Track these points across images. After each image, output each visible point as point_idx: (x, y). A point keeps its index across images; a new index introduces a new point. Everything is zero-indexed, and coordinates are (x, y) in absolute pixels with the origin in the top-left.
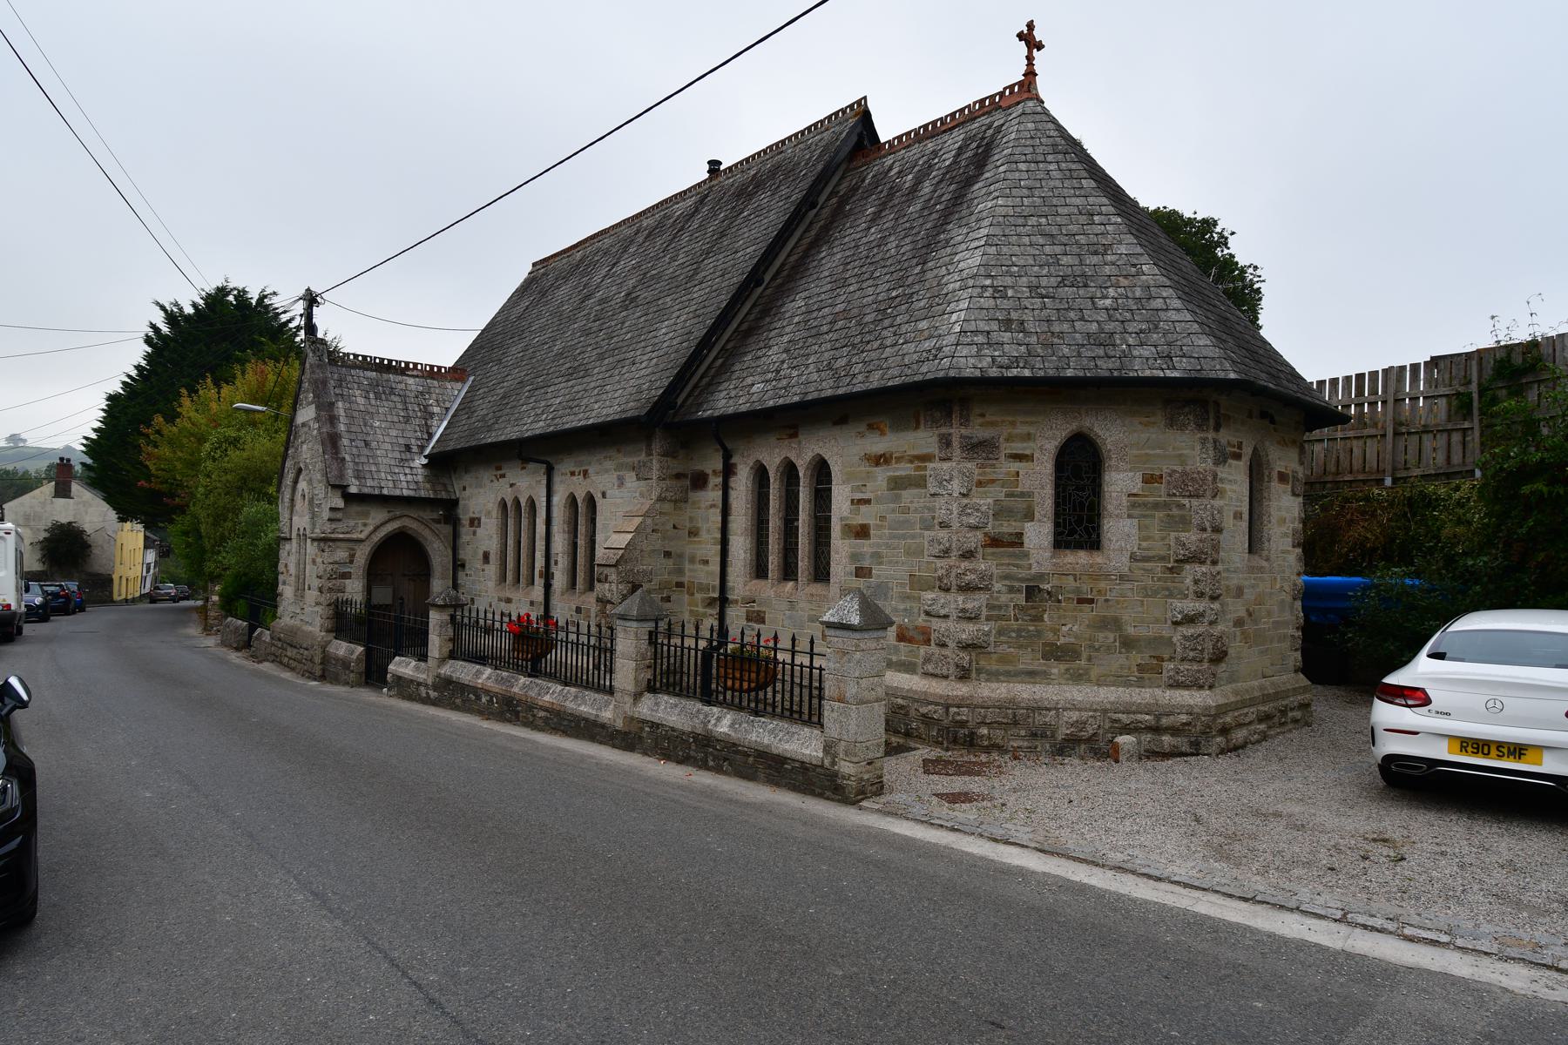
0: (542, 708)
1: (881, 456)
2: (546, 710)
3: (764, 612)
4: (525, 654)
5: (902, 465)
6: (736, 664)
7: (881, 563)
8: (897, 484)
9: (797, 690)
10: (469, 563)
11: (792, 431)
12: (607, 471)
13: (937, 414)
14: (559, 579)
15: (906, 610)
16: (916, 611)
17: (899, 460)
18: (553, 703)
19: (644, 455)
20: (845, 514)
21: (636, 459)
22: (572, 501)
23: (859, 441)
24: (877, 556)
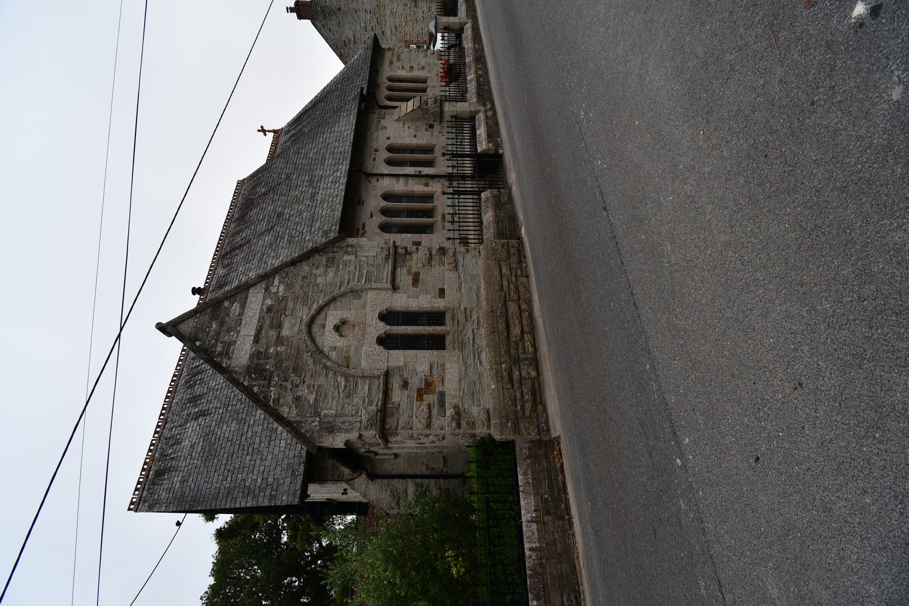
0: (475, 46)
2: (474, 44)
10: (421, 308)
12: (377, 137)
19: (374, 116)
21: (376, 120)
22: (389, 162)
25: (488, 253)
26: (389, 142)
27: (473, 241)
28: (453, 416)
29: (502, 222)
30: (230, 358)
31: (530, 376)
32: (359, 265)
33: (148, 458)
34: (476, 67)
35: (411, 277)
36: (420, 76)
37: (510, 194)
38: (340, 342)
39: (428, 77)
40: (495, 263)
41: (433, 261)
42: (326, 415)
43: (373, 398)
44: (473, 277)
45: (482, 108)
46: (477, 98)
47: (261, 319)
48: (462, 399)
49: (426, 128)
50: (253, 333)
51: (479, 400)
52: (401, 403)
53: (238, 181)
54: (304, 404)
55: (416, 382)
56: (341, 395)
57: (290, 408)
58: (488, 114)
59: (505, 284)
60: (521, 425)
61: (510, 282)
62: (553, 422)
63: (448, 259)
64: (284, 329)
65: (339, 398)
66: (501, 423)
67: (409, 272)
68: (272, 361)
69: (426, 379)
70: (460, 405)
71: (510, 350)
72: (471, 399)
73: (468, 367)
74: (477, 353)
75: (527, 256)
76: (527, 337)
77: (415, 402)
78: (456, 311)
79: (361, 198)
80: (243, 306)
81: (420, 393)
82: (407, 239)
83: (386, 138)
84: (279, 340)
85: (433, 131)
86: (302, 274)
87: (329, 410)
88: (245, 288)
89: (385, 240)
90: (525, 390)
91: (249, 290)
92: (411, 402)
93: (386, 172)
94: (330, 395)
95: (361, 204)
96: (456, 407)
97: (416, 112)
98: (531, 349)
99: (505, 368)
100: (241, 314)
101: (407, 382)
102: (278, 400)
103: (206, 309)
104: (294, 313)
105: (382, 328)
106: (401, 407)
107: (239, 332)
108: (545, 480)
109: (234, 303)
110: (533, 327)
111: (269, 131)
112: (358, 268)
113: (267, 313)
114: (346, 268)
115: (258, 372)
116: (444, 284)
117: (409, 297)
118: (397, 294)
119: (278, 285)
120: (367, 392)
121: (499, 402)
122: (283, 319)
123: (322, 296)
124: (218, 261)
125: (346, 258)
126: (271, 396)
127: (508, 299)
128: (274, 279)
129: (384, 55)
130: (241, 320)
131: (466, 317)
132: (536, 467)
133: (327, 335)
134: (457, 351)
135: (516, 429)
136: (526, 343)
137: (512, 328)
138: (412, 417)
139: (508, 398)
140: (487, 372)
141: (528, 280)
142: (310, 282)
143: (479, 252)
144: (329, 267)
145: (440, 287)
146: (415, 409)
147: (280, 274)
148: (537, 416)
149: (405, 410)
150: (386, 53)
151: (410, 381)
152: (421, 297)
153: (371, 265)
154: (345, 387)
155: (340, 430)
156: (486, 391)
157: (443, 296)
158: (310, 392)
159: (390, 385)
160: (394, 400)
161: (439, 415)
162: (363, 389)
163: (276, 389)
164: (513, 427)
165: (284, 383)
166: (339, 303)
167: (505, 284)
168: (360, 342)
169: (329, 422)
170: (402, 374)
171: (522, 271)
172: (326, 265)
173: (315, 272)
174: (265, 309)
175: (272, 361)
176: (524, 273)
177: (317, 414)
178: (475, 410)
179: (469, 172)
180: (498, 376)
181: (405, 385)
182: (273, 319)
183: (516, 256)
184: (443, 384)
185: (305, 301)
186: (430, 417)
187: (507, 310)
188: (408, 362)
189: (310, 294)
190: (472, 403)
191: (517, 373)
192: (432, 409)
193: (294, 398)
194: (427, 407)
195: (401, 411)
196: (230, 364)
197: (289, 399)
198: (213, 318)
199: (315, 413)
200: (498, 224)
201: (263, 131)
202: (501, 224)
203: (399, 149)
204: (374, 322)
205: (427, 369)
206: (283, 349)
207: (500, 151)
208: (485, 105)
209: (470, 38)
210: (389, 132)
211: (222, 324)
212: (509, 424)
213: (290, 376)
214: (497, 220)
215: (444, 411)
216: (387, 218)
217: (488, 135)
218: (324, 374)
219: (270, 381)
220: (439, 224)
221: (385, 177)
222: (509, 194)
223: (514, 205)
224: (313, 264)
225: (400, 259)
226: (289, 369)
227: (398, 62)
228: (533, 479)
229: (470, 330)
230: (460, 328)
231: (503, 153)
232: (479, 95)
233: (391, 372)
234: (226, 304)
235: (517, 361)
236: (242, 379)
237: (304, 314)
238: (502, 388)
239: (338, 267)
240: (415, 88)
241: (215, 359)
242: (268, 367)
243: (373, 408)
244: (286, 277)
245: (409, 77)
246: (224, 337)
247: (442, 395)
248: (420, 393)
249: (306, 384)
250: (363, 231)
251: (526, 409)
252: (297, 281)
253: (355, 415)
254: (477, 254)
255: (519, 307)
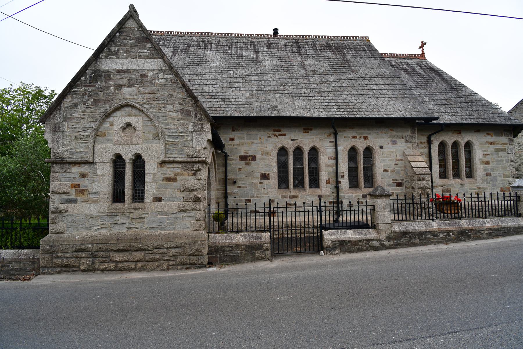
0: (486, 230)
1: (492, 142)
3: (450, 189)
4: (400, 215)
5: (499, 145)
6: (488, 203)
7: (494, 171)
8: (497, 150)
9: (474, 211)
11: (458, 132)
12: (383, 138)
13: (508, 133)
14: (345, 183)
15: (503, 183)
16: (505, 183)
17: (497, 144)
18: (493, 226)
20: (481, 158)
22: (353, 152)
23: (484, 137)
24: (493, 170)
25: (192, 238)
26: (376, 148)
27: (352, 217)
28: (58, 209)
29: (231, 251)
30: (106, 57)
31: (81, 265)
32: (184, 135)
33: (164, 33)
34: (451, 231)
35: (172, 175)
36: (476, 172)
37: (263, 259)
38: (117, 128)
39: (476, 180)
40: (181, 244)
41: (188, 193)
42: (64, 125)
43: (75, 155)
44: (173, 224)
45: (383, 236)
46: (399, 231)
47: (136, 71)
48: (72, 215)
49: (397, 180)
50: (125, 68)
51: (71, 226)
52: (71, 174)
53: (368, 37)
54: (72, 110)
55: (84, 183)
56: (77, 134)
57: (70, 102)
58: (374, 242)
59: (161, 251)
60: (47, 255)
61: (163, 255)
62: (43, 278)
63: (190, 204)
64: (127, 88)
65: (75, 132)
66: (50, 241)
67: (176, 174)
68: (103, 84)
69: (86, 190)
70: (68, 214)
71: (103, 251)
72: (71, 221)
73: (96, 219)
74: (105, 226)
75: (188, 270)
76: (113, 265)
77: (70, 183)
78: (141, 211)
79: (311, 130)
80: (147, 57)
81: (76, 186)
82: (271, 169)
83: (381, 145)
84: (119, 87)
85: (393, 186)
86: (175, 94)
87: (67, 127)
88: (161, 56)
89: (270, 152)
90: (70, 260)
91: (160, 58)
92: (70, 181)
93: (339, 148)
94: (77, 126)
95: (304, 131)
96: (66, 211)
97: (412, 170)
98: (102, 267)
99: (88, 247)
100: (140, 57)
101: (85, 177)
102: (76, 94)
103: (145, 33)
104: (141, 93)
105: (128, 156)
106: (68, 173)
107: (126, 58)
108: (20, 267)
109: (149, 50)
110: (122, 270)
111: (423, 50)
112: (182, 134)
113: (141, 74)
114: (180, 125)
115: (96, 78)
116: (166, 201)
117: (154, 175)
118: (156, 166)
119: (165, 78)
120: (79, 150)
121: (64, 241)
122: (136, 87)
123: (156, 110)
124: (294, 39)
125: (191, 125)
126: (78, 89)
127: (147, 252)
128: (170, 74)
129: (502, 136)
130: (136, 58)
131: (136, 218)
132: (27, 262)
133: (122, 118)
134: (107, 212)
135: (46, 252)
136: (108, 264)
137: (120, 254)
138: (61, 181)
139: (65, 248)
140: (91, 233)
141: (164, 270)
142: (167, 101)
143: (196, 230)
144: (181, 113)
145: (163, 199)
146: (65, 183)
147: (174, 78)
148: (54, 267)
149: (66, 176)
150: (505, 138)
151: (86, 178)
152: (154, 184)
153: (184, 144)
154: (83, 136)
155: (54, 135)
156: (78, 232)
157: (155, 200)
158: (80, 113)
159: (82, 165)
160: (73, 168)
161: (61, 199)
162: (81, 147)
163: (83, 91)
164: (46, 250)
165: (87, 95)
166: (149, 123)
167: (161, 251)
168: (116, 142)
169: (59, 128)
170: (91, 173)
171: (174, 265)
172: (183, 111)
173: (177, 103)
174: (144, 72)
175: (103, 84)
176: (172, 267)
177: (65, 120)
178: (63, 224)
179: (344, 219)
180: (84, 241)
181: (83, 176)
182: (136, 79)
183: (188, 261)
184: (82, 201)
185: (152, 100)
186: (59, 193)
187: (136, 251)
188: (99, 177)
189: (157, 102)
190: (69, 222)
191: (84, 255)
192: (65, 194)
193: (76, 103)
194: (66, 191)
195: (65, 174)
196: (102, 58)
197: (76, 101)
198: (138, 40)
199: (66, 118)
200: (228, 247)
201: (423, 44)
202: (228, 249)
203: (371, 157)
204: (132, 151)
205: (94, 190)
206: (112, 90)
207: (322, 252)
208: (388, 239)
209: (501, 224)
210: (389, 147)
211: (132, 46)
212: (48, 247)
213: (92, 98)
214: (233, 247)
215: (63, 202)
216: (362, 153)
217: (344, 241)
218: (92, 120)
219: (89, 86)
220: (286, 193)
221: (335, 148)
222: (264, 258)
223: (252, 262)
224: (184, 100)
225: (188, 166)
226: (97, 97)
227: (494, 150)
228: (20, 259)
229: (124, 222)
230: (127, 214)
231: (320, 254)
232: (404, 234)
233: (93, 165)
234: (149, 45)
235: (93, 256)
236: (91, 68)
237: (141, 99)
238: (74, 243)
239: (182, 119)
240: (460, 167)
241: (106, 48)
242: (99, 83)
243: (67, 155)
244: (172, 83)
245: (474, 161)
246: (122, 50)
247: (75, 201)
248: (76, 186)
249: (86, 110)
250: (277, 135)
251: (57, 259)
252: (168, 91)
253: (63, 144)
254: (195, 228)
255: (138, 261)
